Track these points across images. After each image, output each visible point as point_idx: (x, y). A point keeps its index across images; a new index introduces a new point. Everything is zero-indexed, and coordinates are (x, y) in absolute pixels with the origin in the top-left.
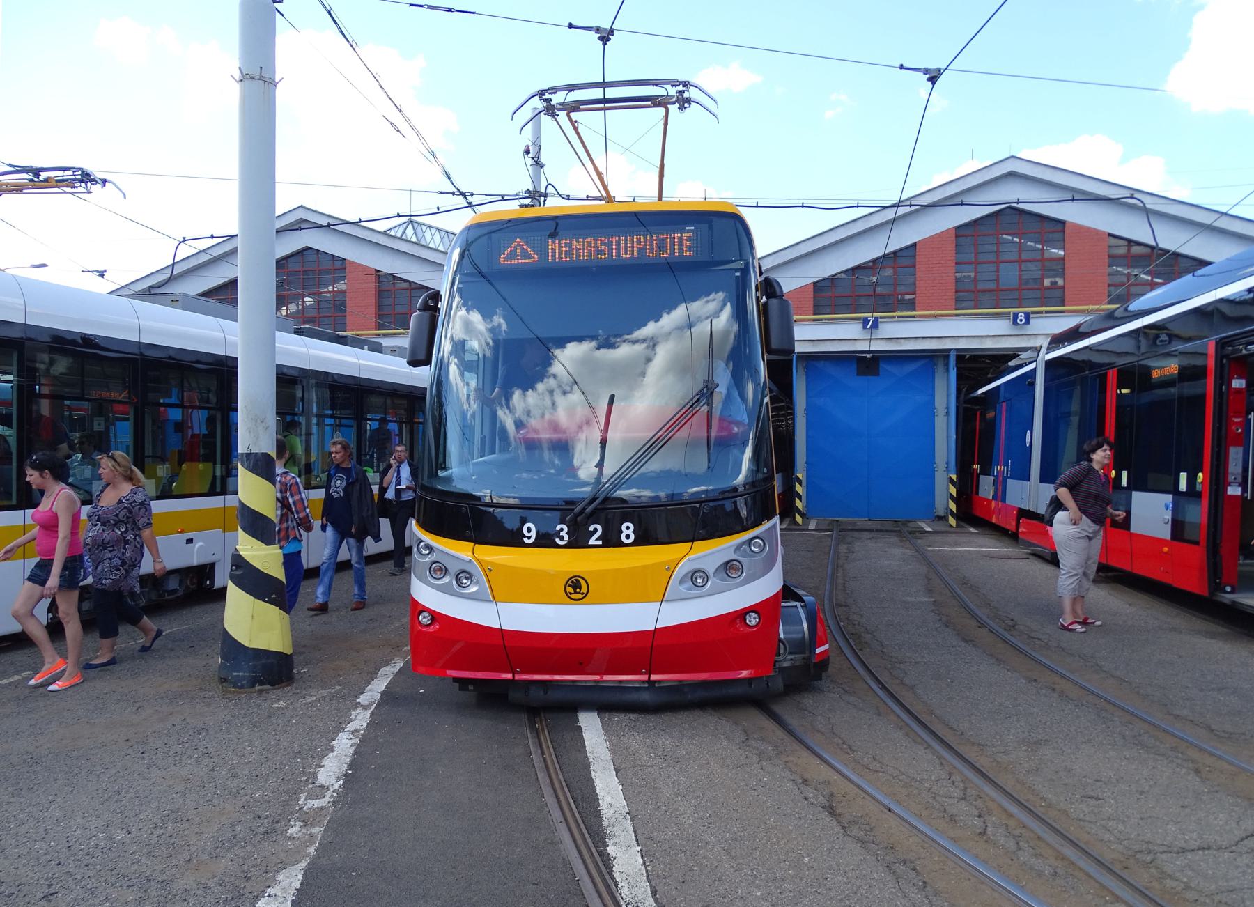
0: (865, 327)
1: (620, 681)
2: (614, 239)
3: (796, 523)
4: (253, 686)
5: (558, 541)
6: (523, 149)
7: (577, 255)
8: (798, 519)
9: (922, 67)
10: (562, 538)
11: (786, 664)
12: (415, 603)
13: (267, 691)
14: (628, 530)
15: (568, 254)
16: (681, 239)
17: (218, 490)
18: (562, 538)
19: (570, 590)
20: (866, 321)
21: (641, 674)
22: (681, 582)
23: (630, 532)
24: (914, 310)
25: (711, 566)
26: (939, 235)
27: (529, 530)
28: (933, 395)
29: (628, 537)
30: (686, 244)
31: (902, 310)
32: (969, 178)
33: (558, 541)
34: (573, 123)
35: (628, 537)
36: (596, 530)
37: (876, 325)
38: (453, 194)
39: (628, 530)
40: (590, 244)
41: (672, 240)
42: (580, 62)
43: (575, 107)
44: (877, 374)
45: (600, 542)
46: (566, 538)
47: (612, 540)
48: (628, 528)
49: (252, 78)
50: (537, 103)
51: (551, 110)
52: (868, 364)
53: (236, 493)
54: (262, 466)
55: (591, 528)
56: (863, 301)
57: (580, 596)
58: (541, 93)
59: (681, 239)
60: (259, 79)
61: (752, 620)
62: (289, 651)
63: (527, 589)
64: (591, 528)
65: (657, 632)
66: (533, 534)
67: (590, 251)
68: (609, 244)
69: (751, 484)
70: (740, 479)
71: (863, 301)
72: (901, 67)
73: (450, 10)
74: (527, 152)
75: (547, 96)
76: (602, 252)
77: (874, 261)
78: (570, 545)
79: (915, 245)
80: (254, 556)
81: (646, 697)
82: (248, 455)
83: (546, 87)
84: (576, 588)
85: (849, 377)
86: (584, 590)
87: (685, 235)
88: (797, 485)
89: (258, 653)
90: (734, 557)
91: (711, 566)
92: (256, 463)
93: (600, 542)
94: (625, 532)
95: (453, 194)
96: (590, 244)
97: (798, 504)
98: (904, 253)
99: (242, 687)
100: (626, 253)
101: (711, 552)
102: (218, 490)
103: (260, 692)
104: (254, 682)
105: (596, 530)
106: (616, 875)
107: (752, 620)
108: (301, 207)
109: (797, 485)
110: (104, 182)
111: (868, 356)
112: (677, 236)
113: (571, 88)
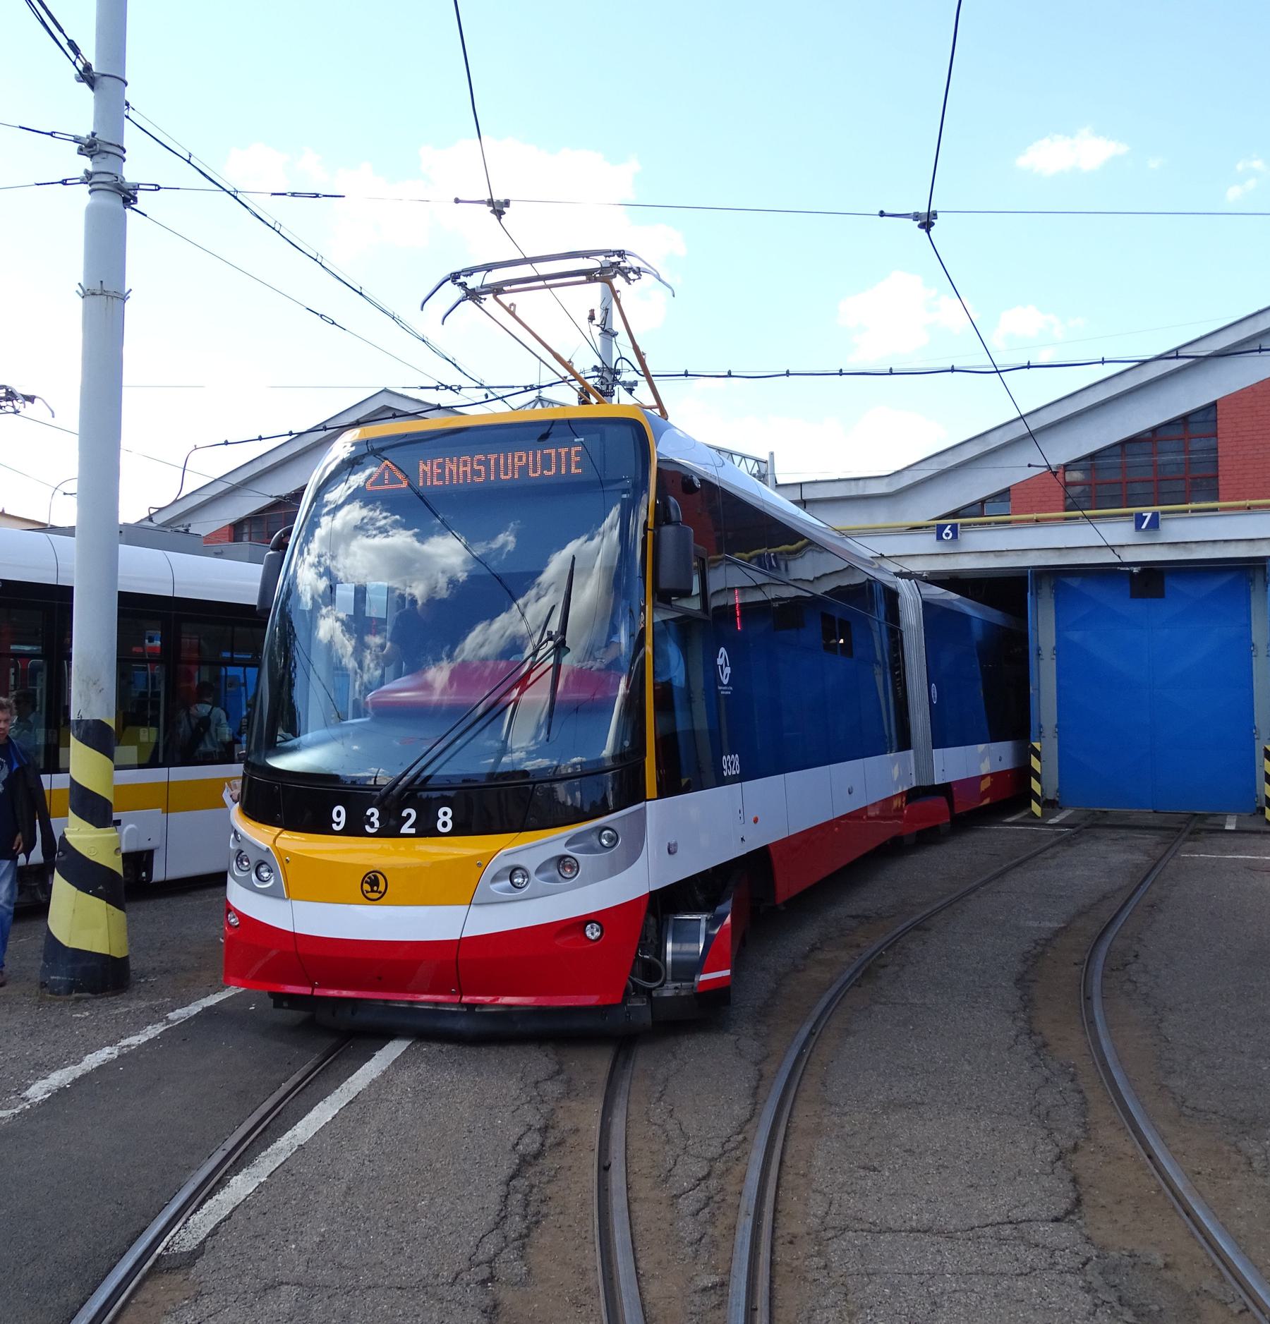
0: (1138, 527)
1: (437, 1003)
2: (492, 457)
3: (1033, 815)
4: (70, 993)
5: (368, 828)
6: (588, 314)
7: (425, 482)
8: (1036, 808)
9: (911, 211)
10: (372, 825)
11: (667, 993)
12: (228, 903)
13: (87, 999)
14: (445, 816)
15: (441, 477)
16: (568, 454)
17: (161, 760)
18: (372, 825)
19: (367, 887)
20: (1139, 519)
21: (452, 994)
22: (495, 879)
23: (448, 819)
24: (1217, 499)
25: (531, 861)
26: (1252, 389)
27: (339, 814)
28: (1249, 625)
29: (445, 824)
30: (574, 459)
31: (1198, 501)
32: (255, 463)
33: (368, 828)
34: (511, 310)
35: (445, 824)
36: (409, 815)
37: (1155, 523)
38: (437, 388)
39: (445, 816)
40: (520, 458)
41: (558, 455)
42: (484, 242)
43: (497, 289)
44: (1160, 594)
45: (413, 831)
46: (377, 824)
47: (426, 829)
48: (445, 814)
49: (93, 294)
50: (452, 292)
51: (473, 295)
52: (1150, 580)
53: (67, 771)
54: (98, 737)
55: (404, 814)
56: (1138, 488)
57: (376, 895)
58: (454, 277)
59: (568, 454)
60: (105, 295)
61: (592, 932)
62: (118, 954)
63: (320, 883)
64: (404, 814)
65: (464, 942)
66: (343, 819)
67: (465, 472)
68: (486, 463)
69: (618, 757)
70: (607, 752)
71: (1138, 488)
72: (882, 214)
73: (317, 196)
74: (592, 318)
75: (462, 279)
76: (478, 473)
77: (1154, 430)
78: (346, 832)
79: (1214, 404)
80: (79, 841)
81: (461, 1025)
82: (79, 722)
83: (459, 269)
84: (373, 886)
85: (1119, 601)
86: (382, 888)
87: (573, 450)
88: (1033, 758)
89: (78, 954)
90: (566, 851)
91: (531, 861)
92: (86, 733)
93: (413, 831)
94: (442, 819)
95: (437, 388)
96: (520, 458)
97: (1036, 786)
98: (1199, 417)
99: (58, 994)
100: (535, 471)
101: (535, 847)
102: (161, 760)
103: (78, 1000)
104: (72, 987)
105: (409, 815)
106: (210, 1203)
107: (592, 932)
108: (385, 390)
109: (1033, 758)
110: (31, 399)
111: (1135, 570)
112: (563, 451)
113: (489, 268)
